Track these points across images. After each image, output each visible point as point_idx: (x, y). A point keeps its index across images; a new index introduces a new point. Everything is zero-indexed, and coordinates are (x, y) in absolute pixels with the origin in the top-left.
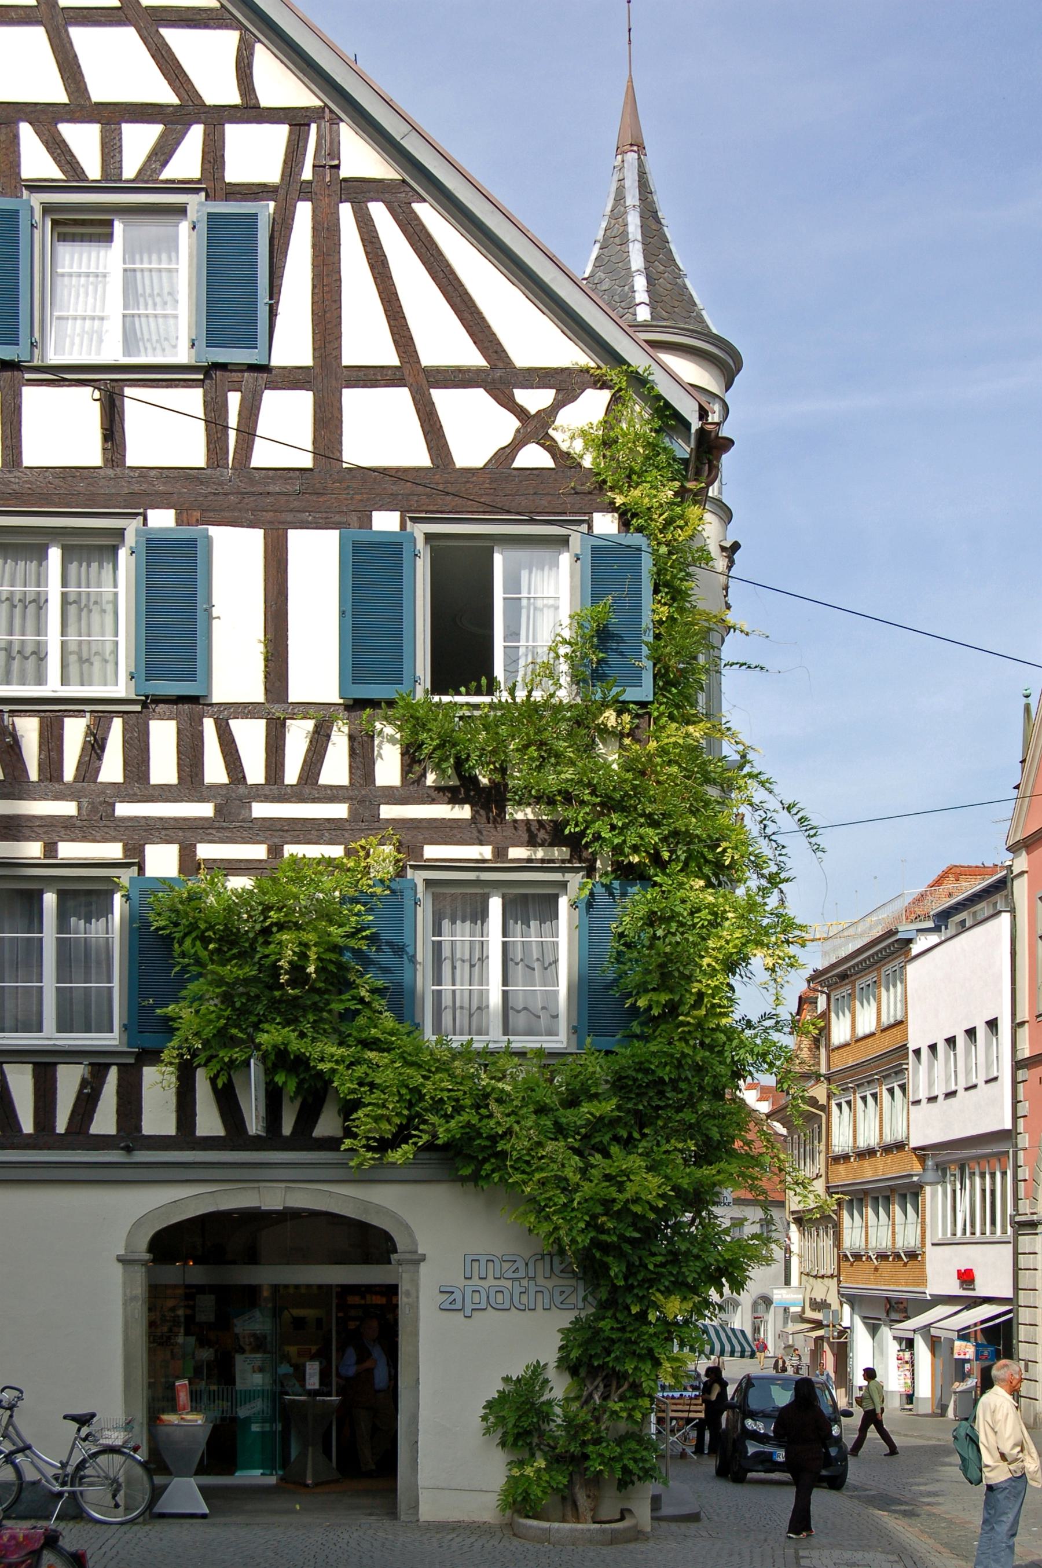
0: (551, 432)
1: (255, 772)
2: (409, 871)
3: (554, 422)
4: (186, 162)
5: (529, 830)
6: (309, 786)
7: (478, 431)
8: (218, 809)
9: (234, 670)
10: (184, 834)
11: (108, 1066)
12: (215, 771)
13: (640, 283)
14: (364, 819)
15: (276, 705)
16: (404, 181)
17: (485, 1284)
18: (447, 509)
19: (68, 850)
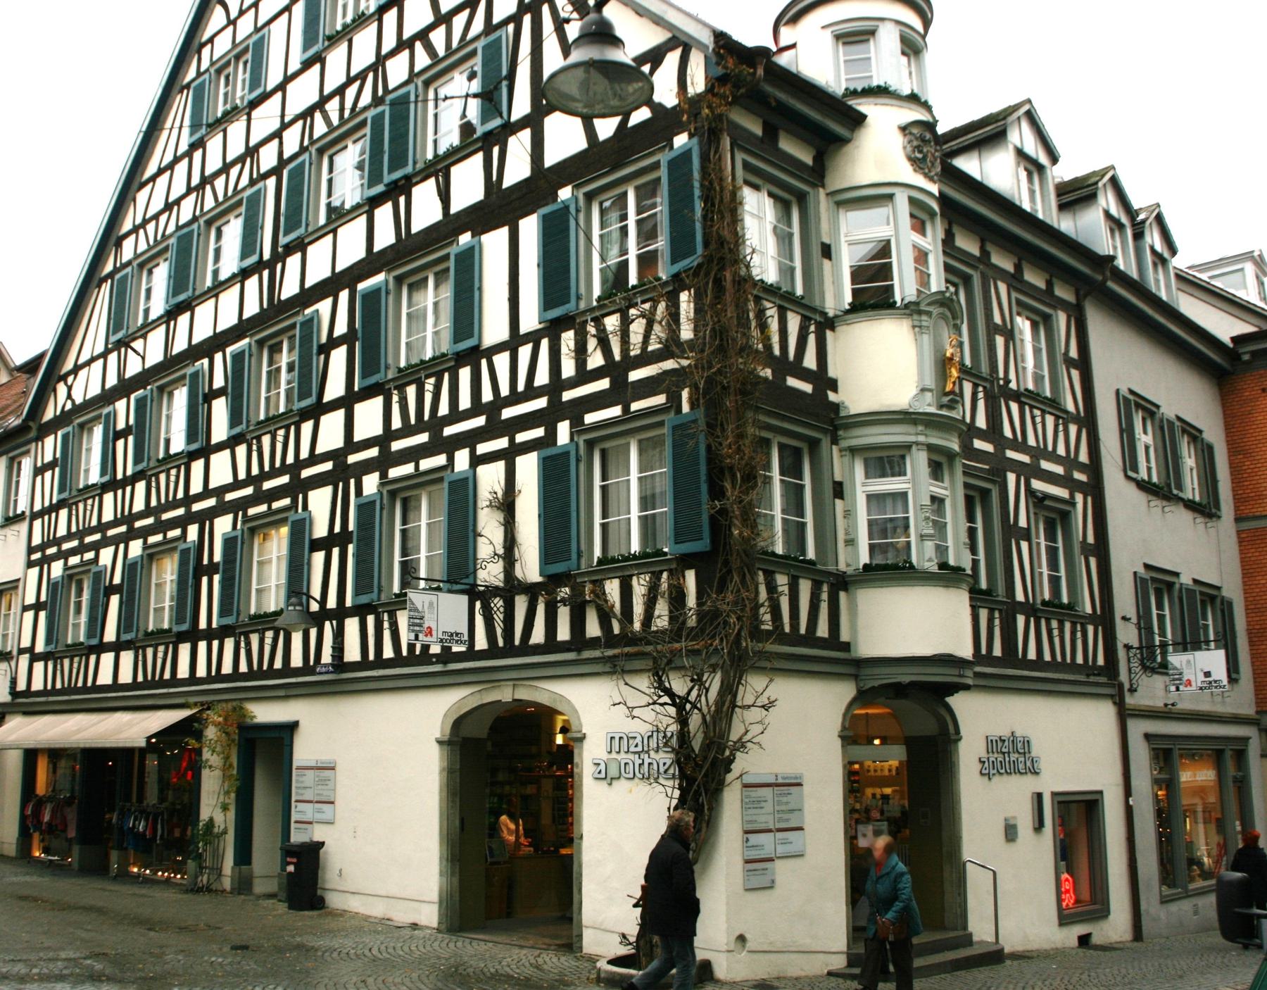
1: (505, 391)
4: (478, 26)
6: (531, 392)
8: (546, 430)
9: (494, 329)
11: (661, 572)
12: (487, 396)
15: (512, 344)
17: (619, 757)
19: (426, 464)
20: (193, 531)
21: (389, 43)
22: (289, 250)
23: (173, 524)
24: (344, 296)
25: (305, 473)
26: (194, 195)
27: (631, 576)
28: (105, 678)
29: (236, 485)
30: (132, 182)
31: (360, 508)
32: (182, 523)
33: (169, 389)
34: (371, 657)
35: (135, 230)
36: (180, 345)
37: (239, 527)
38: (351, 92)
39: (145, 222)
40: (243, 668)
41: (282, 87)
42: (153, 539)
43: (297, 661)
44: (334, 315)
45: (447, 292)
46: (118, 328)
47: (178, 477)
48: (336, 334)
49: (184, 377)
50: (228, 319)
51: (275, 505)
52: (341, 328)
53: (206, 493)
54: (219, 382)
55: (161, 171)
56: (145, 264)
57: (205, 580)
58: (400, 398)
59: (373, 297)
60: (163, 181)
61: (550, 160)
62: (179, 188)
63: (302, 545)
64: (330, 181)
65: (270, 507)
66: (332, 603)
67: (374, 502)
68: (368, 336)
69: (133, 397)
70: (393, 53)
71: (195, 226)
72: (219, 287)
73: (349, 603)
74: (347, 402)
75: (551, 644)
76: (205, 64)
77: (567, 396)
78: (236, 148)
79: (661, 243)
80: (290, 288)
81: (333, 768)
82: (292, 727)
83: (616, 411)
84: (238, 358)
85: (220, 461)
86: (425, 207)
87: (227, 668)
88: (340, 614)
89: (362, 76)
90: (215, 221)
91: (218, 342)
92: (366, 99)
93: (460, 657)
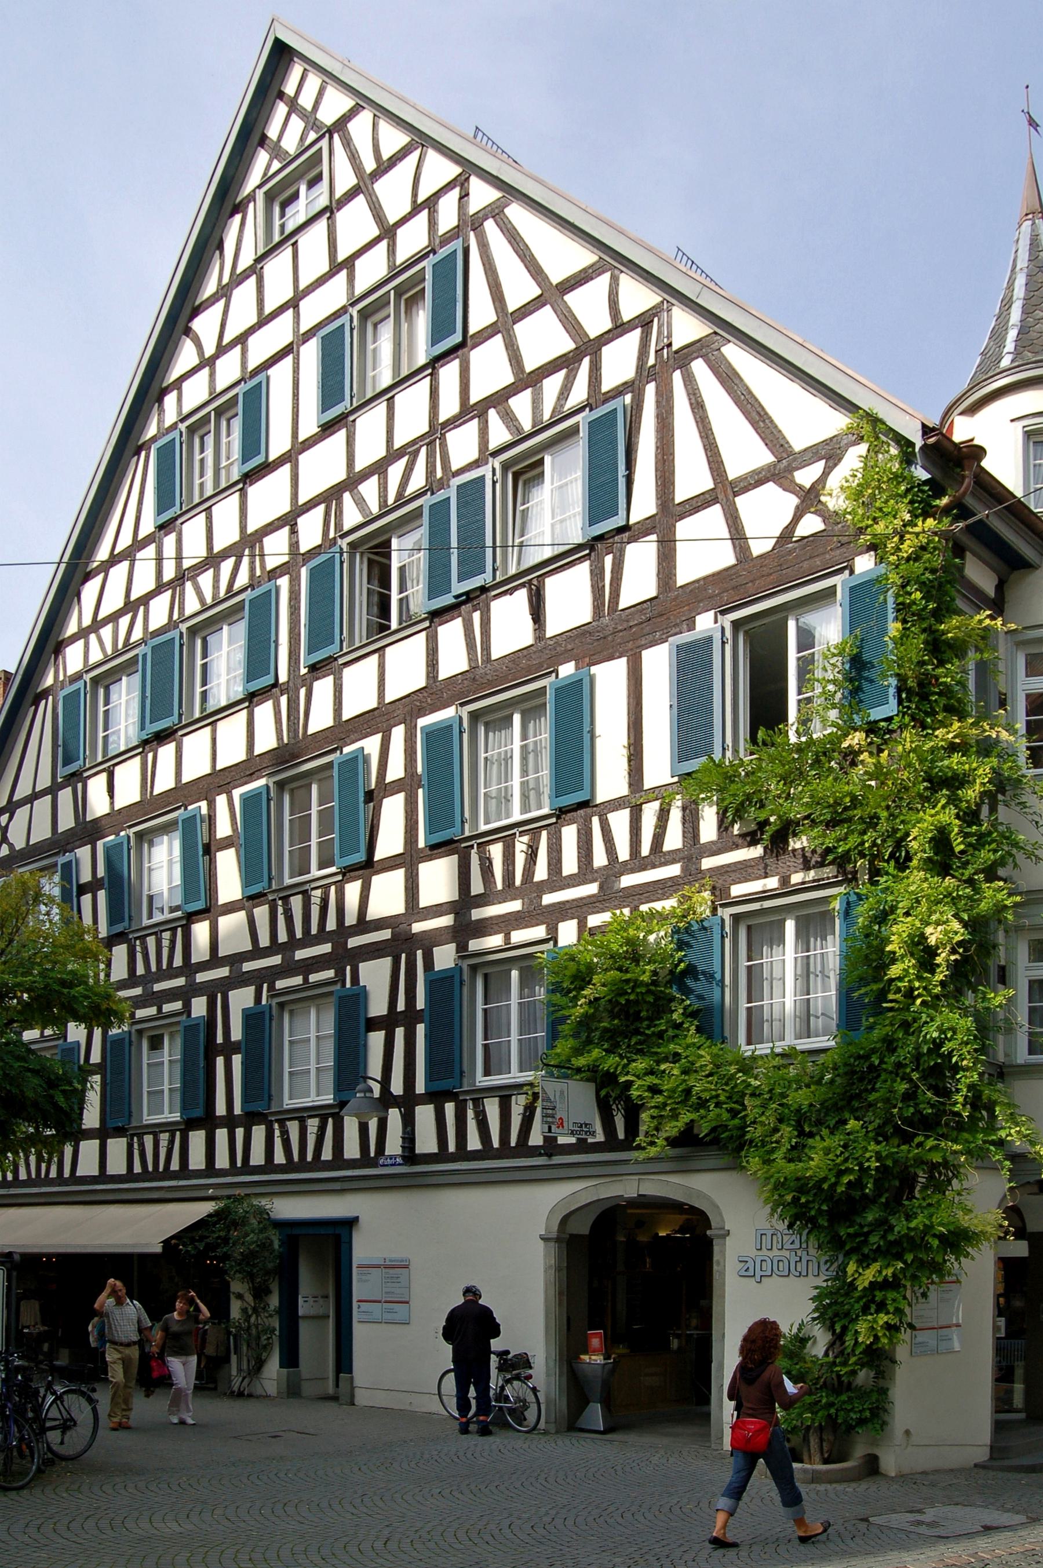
0: (823, 499)
1: (623, 853)
2: (719, 909)
3: (824, 488)
4: (579, 393)
5: (804, 856)
6: (659, 856)
7: (767, 513)
9: (610, 780)
10: (578, 910)
12: (600, 859)
13: (1012, 334)
14: (692, 874)
16: (715, 333)
17: (771, 1254)
18: (746, 595)
19: (518, 936)
20: (199, 1007)
21: (449, 407)
22: (316, 669)
23: (171, 995)
24: (398, 733)
25: (353, 942)
26: (167, 596)
27: (511, 1096)
28: (88, 1167)
29: (257, 952)
30: (77, 570)
31: (430, 985)
32: (185, 995)
33: (149, 837)
34: (452, 1148)
35: (83, 634)
36: (165, 781)
37: (264, 1002)
38: (395, 472)
39: (96, 625)
40: (279, 1158)
41: (290, 458)
42: (594, 920)
43: (352, 1150)
44: (393, 755)
45: (544, 733)
46: (68, 761)
47: (173, 942)
48: (389, 779)
49: (174, 823)
50: (232, 754)
51: (313, 978)
52: (396, 771)
53: (215, 960)
54: (223, 829)
55: (114, 560)
56: (104, 680)
57: (220, 1061)
58: (284, 909)
59: (438, 737)
60: (119, 572)
61: (684, 575)
62: (144, 583)
63: (352, 1022)
64: (205, 667)
65: (306, 980)
66: (397, 1087)
67: (124, 1039)
68: (440, 777)
69: (100, 844)
70: (454, 422)
71: (174, 634)
72: (212, 718)
73: (420, 1088)
74: (408, 861)
75: (269, 1165)
76: (170, 416)
77: (707, 863)
78: (226, 535)
79: (545, 774)
80: (320, 719)
81: (406, 1267)
82: (350, 1224)
83: (772, 883)
84: (248, 801)
85: (231, 923)
86: (510, 625)
87: (257, 1158)
88: (408, 1103)
89: (410, 451)
90: (204, 628)
91: (219, 781)
92: (418, 480)
93: (568, 1149)
